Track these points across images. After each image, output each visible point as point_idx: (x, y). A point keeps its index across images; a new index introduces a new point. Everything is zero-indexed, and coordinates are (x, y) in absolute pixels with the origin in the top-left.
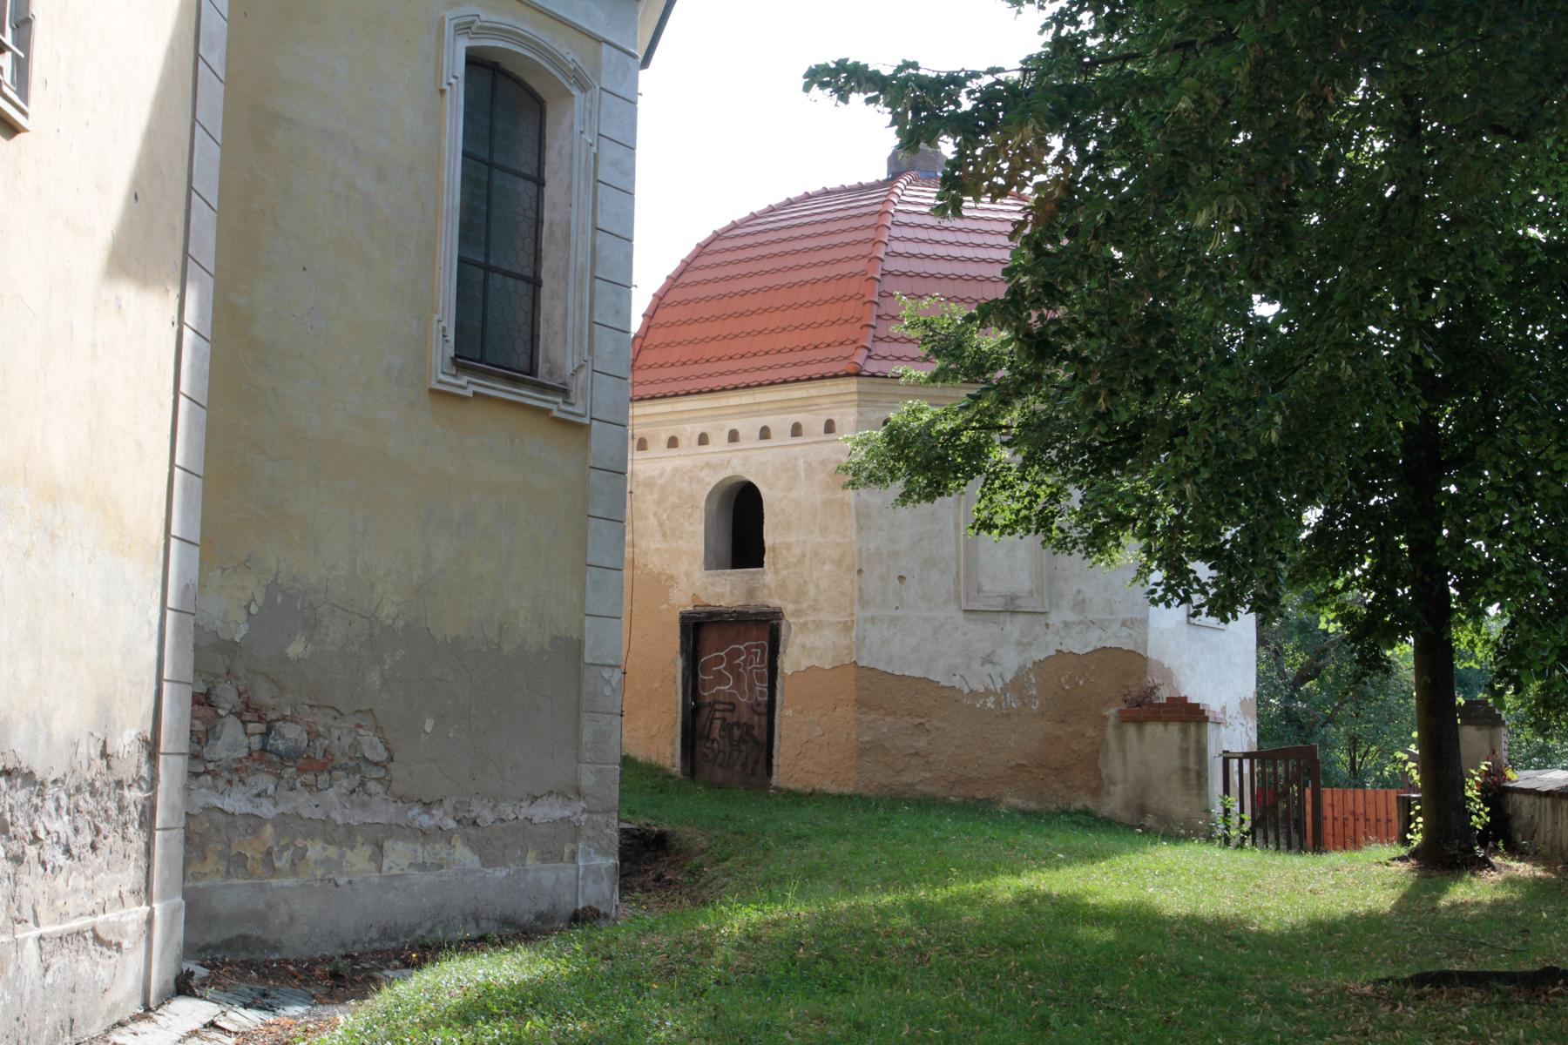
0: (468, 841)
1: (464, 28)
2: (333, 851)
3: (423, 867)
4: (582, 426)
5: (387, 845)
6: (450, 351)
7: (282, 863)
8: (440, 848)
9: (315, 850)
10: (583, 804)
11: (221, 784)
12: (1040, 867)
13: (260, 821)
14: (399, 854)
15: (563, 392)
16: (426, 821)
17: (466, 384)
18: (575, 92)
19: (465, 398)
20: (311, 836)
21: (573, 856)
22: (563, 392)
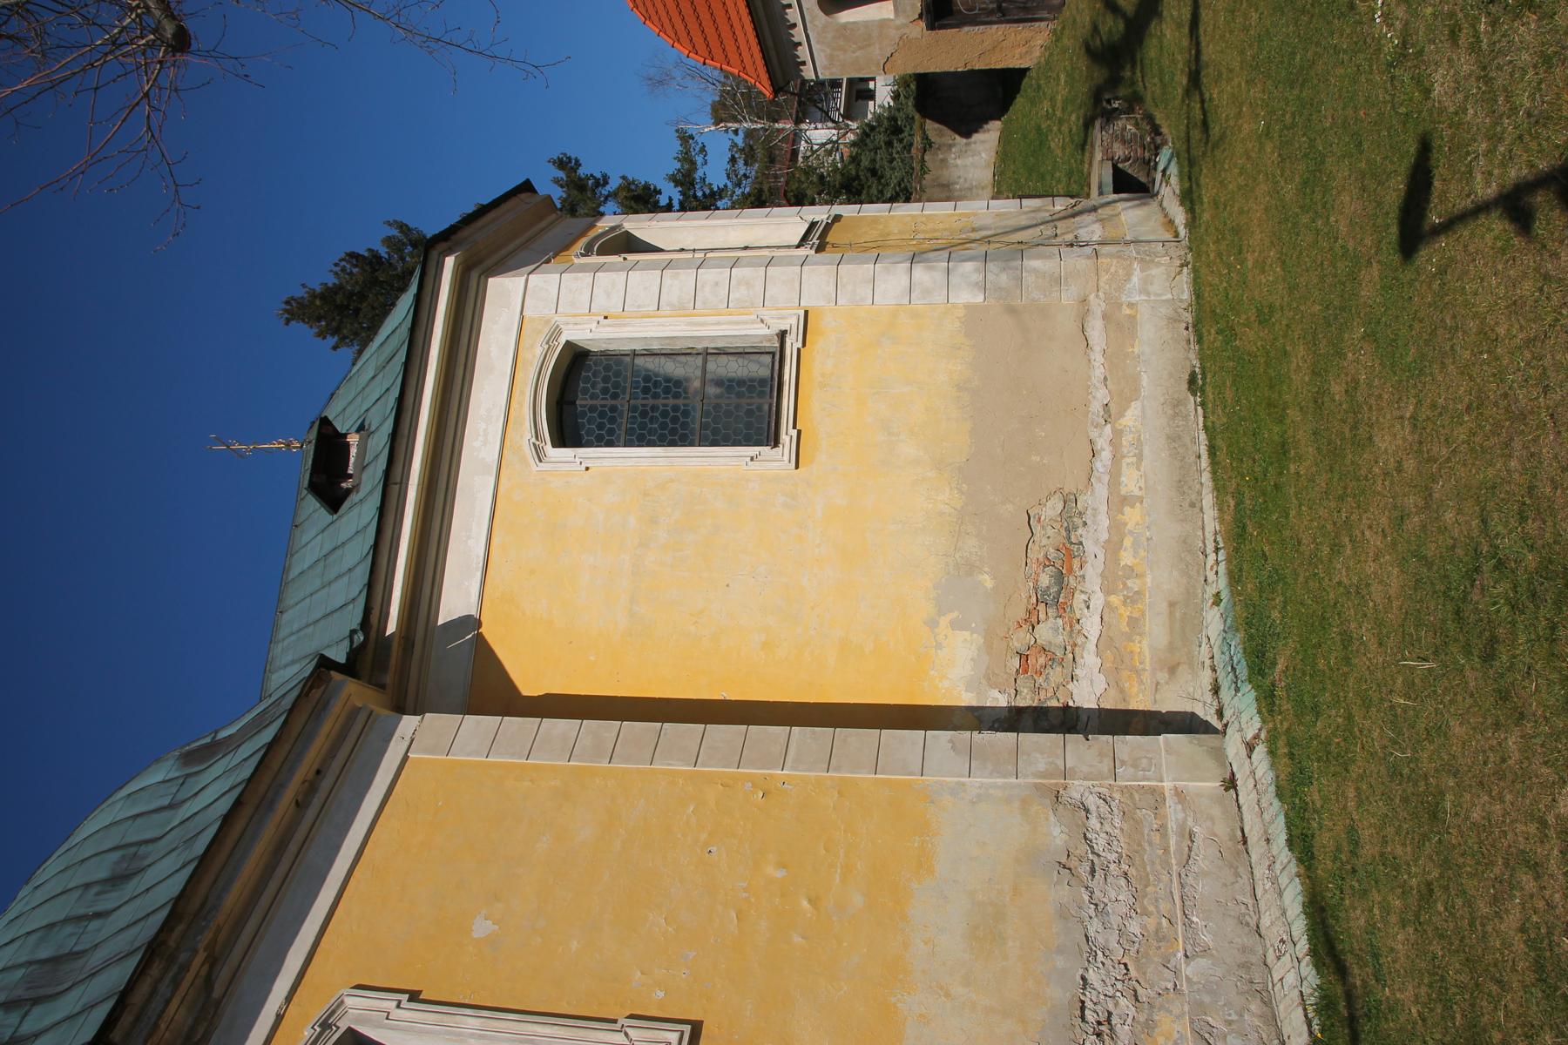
0: (1121, 415)
1: (540, 455)
2: (1128, 542)
3: (1140, 457)
4: (806, 313)
5: (1123, 491)
6: (765, 450)
7: (1134, 584)
8: (1126, 440)
9: (1127, 558)
10: (1092, 297)
11: (1080, 640)
12: (657, 375)
13: (1107, 604)
14: (1130, 482)
15: (782, 335)
16: (1106, 455)
17: (787, 435)
18: (562, 341)
19: (799, 432)
20: (1117, 561)
21: (1131, 305)
22: (782, 335)
